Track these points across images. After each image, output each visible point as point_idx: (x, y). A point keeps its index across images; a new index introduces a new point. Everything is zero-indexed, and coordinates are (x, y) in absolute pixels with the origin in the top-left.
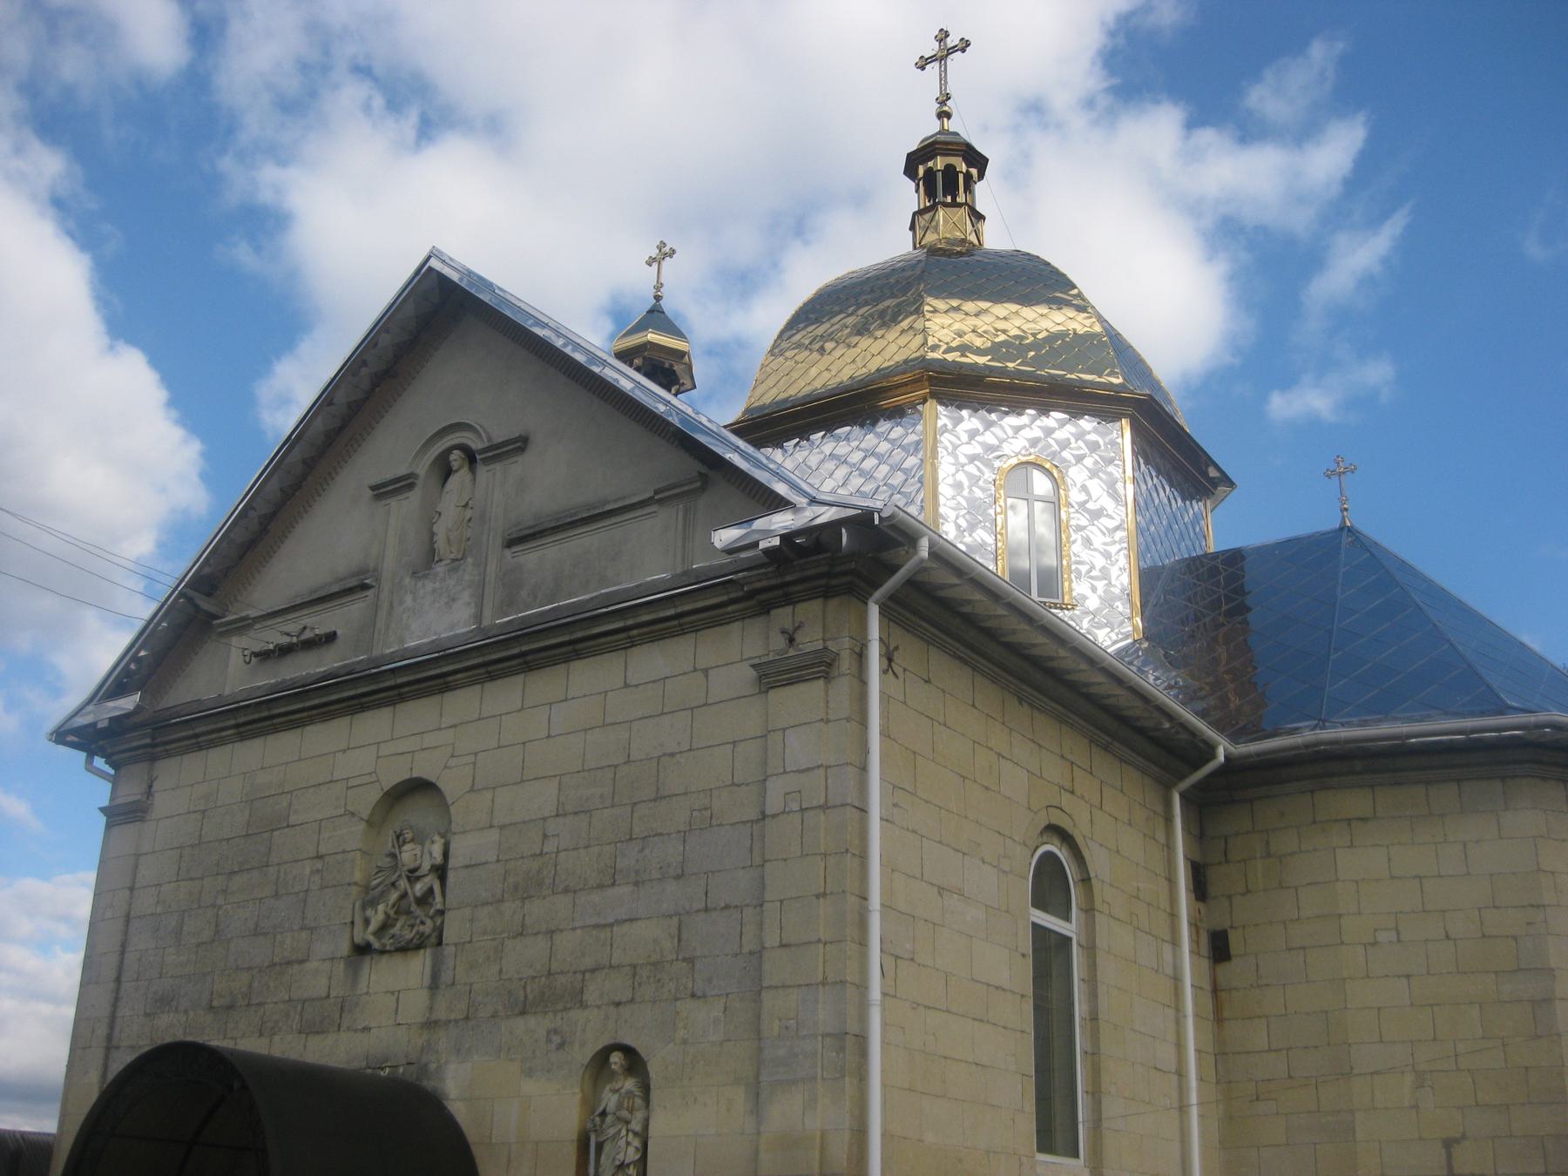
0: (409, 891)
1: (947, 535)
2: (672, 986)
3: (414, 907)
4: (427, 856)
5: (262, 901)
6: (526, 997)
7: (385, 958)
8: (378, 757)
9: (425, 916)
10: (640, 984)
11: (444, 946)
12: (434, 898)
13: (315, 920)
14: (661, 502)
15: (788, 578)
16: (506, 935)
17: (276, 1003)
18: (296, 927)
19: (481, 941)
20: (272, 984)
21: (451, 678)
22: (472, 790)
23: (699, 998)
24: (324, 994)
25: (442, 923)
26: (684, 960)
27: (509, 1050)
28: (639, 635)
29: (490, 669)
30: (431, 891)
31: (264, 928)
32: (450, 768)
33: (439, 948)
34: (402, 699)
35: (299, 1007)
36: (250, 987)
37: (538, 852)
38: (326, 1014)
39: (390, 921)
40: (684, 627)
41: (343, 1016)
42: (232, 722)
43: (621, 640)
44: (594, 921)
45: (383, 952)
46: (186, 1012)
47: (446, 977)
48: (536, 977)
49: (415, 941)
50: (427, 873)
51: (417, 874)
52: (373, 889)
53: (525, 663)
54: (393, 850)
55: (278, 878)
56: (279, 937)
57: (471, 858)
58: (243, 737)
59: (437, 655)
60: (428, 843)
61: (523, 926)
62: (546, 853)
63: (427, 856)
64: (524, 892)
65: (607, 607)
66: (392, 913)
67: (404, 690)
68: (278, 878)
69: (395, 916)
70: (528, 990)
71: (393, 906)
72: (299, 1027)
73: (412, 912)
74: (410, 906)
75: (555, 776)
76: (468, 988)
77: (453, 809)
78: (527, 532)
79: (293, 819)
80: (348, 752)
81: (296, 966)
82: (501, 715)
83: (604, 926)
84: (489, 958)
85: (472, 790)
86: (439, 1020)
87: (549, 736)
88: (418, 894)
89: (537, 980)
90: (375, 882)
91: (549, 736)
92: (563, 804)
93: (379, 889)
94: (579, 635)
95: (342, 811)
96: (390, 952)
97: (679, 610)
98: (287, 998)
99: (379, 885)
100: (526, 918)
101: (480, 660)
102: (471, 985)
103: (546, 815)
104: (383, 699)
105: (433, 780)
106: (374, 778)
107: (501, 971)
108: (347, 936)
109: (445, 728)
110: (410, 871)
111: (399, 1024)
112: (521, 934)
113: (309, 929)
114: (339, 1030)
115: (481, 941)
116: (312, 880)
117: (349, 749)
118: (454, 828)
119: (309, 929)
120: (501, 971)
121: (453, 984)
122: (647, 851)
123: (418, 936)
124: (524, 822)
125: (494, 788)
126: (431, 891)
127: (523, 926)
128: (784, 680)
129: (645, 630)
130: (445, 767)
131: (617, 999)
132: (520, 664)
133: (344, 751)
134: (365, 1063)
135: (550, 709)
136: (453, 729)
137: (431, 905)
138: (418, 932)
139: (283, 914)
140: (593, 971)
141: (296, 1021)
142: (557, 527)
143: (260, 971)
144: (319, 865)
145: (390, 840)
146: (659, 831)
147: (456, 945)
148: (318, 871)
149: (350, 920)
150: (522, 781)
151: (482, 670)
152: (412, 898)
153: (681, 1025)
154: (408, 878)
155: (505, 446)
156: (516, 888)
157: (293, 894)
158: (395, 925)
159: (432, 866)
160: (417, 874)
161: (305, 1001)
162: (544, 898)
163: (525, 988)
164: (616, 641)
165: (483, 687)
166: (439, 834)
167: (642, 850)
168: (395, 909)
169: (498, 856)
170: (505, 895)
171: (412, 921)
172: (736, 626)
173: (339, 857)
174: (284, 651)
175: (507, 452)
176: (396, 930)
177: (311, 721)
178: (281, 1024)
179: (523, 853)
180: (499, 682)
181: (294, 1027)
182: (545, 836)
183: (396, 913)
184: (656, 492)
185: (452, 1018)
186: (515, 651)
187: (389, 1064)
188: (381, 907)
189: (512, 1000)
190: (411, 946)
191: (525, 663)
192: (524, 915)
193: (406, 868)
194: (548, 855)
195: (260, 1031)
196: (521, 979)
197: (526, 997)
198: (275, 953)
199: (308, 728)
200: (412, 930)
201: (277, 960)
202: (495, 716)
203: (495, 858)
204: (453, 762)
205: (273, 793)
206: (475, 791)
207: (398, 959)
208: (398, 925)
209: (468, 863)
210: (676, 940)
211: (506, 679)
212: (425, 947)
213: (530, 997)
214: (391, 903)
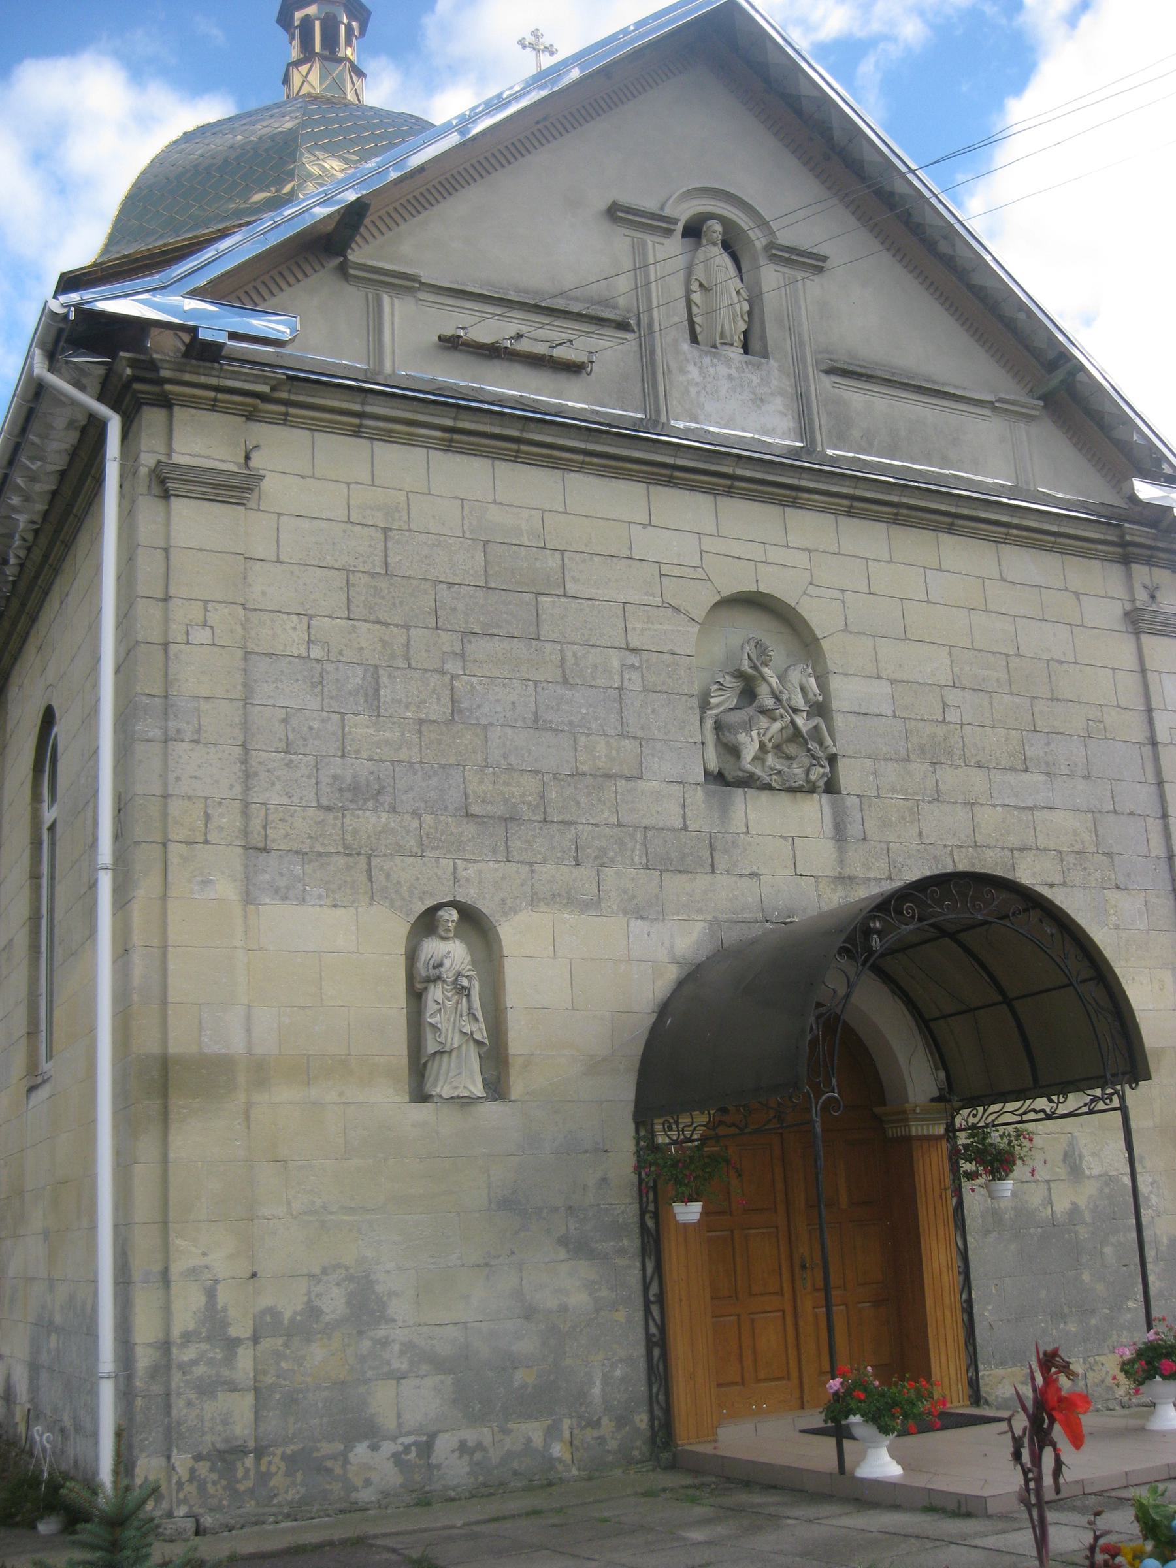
2: (1098, 875)
7: (765, 796)
10: (1068, 869)
14: (994, 409)
15: (1161, 544)
17: (597, 825)
20: (583, 800)
23: (1123, 889)
26: (1104, 854)
28: (1017, 536)
34: (729, 492)
36: (543, 797)
38: (687, 851)
42: (449, 423)
43: (999, 533)
44: (1012, 801)
45: (768, 787)
46: (416, 814)
47: (854, 829)
48: (962, 847)
58: (449, 447)
59: (891, 480)
61: (937, 791)
65: (1010, 499)
67: (524, 448)
78: (858, 370)
81: (622, 783)
83: (1024, 808)
89: (963, 850)
92: (959, 677)
94: (966, 512)
97: (1062, 530)
100: (940, 783)
101: (851, 491)
102: (888, 843)
104: (702, 482)
107: (920, 834)
111: (801, 875)
112: (937, 800)
114: (713, 872)
120: (920, 834)
122: (1053, 746)
127: (937, 791)
128: (1155, 629)
129: (1025, 534)
131: (1049, 881)
139: (584, 711)
140: (1021, 850)
142: (890, 381)
144: (633, 659)
146: (1061, 731)
151: (846, 502)
153: (1112, 912)
155: (808, 258)
163: (952, 854)
164: (878, 512)
167: (1048, 744)
172: (1096, 564)
174: (493, 352)
175: (804, 263)
177: (581, 468)
181: (636, 859)
184: (1000, 400)
186: (895, 499)
191: (896, 514)
195: (576, 859)
199: (572, 475)
201: (582, 768)
204: (812, 590)
207: (785, 798)
209: (857, 709)
210: (1094, 835)
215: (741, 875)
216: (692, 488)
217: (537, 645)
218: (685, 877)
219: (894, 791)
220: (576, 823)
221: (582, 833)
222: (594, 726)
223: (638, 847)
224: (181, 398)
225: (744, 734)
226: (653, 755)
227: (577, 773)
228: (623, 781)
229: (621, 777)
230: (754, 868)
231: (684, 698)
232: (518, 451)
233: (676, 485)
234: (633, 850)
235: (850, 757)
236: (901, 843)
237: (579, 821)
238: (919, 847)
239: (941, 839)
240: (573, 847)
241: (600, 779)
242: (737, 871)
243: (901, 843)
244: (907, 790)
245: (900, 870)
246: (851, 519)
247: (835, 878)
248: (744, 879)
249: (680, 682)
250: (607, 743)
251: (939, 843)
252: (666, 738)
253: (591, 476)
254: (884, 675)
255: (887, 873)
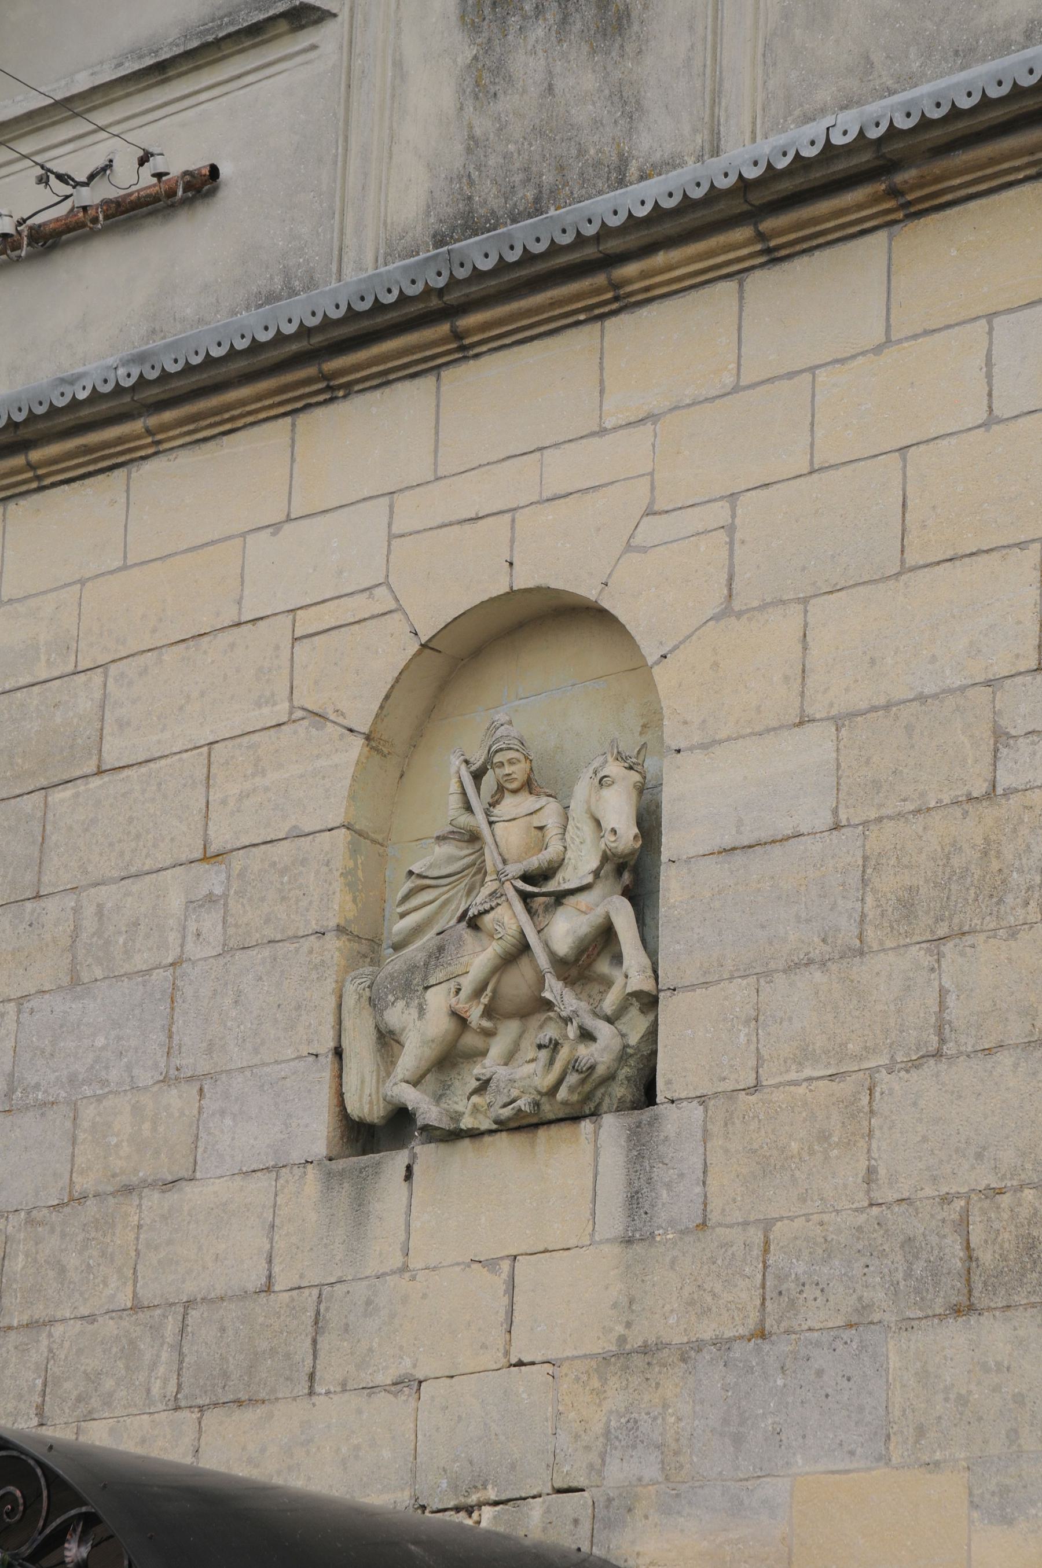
0: (532, 938)
1: (827, 462)
3: (554, 989)
4: (581, 829)
5: (27, 1006)
6: (970, 1257)
8: (391, 537)
9: (596, 1014)
11: (662, 1108)
12: (618, 959)
13: (209, 1050)
16: (884, 1060)
17: (91, 1318)
18: (145, 1078)
19: (795, 1083)
20: (72, 1261)
21: (631, 269)
22: (727, 611)
24: (255, 1279)
25: (652, 1033)
27: (921, 1431)
29: (768, 225)
30: (606, 934)
31: (37, 1087)
32: (644, 550)
33: (647, 1113)
35: (171, 1326)
37: (979, 788)
39: (470, 1040)
40: (467, 342)
41: (323, 1343)
48: (1001, 1192)
49: (562, 1094)
50: (590, 879)
51: (552, 886)
52: (397, 947)
53: (894, 192)
54: (464, 819)
55: (75, 937)
56: (89, 1113)
57: (740, 823)
60: (582, 790)
62: (1008, 793)
63: (581, 829)
64: (939, 919)
66: (475, 1014)
68: (75, 937)
69: (486, 1024)
70: (977, 1235)
71: (478, 992)
72: (172, 1388)
73: (548, 1005)
74: (541, 982)
75: (1021, 545)
76: (756, 1236)
77: (664, 678)
79: (114, 751)
80: (287, 527)
81: (153, 1199)
82: (812, 369)
84: (824, 1137)
85: (727, 611)
86: (661, 1346)
87: (991, 421)
88: (563, 946)
89: (1005, 1200)
90: (402, 926)
91: (991, 421)
93: (428, 939)
95: (281, 711)
96: (474, 1134)
98: (125, 1299)
99: (417, 931)
100: (951, 1001)
102: (767, 1225)
103: (1002, 669)
105: (588, 590)
106: (383, 601)
108: (324, 1097)
109: (615, 429)
110: (526, 878)
111: (520, 1364)
112: (938, 1054)
113: (190, 1079)
115: (795, 1083)
116: (192, 927)
117: (289, 519)
118: (672, 734)
119: (190, 1079)
121: (703, 1225)
123: (573, 1079)
124: (922, 698)
125: (805, 601)
126: (606, 934)
130: (629, 548)
132: (876, 200)
133: (275, 527)
134: (407, 1494)
135: (990, 332)
136: (649, 427)
137: (607, 983)
138: (573, 1066)
139: (100, 1041)
141: (161, 1370)
143: (30, 1222)
144: (213, 879)
145: (454, 787)
147: (702, 1099)
148: (210, 899)
149: (332, 1044)
150: (905, 569)
152: (543, 960)
154: (526, 897)
156: (907, 905)
157: (129, 975)
158: (484, 1053)
159: (605, 858)
160: (552, 886)
161: (189, 1304)
162: (1013, 933)
163: (963, 1223)
164: (992, 161)
165: (741, 285)
166: (620, 757)
168: (485, 1000)
169: (835, 812)
170: (870, 933)
171: (551, 1032)
173: (281, 852)
176: (489, 1065)
178: (109, 1384)
179: (922, 795)
180: (799, 265)
181: (156, 1390)
182: (1001, 737)
183: (489, 1012)
185: (708, 1335)
187: (492, 1495)
188: (438, 1000)
189: (918, 1268)
190: (548, 1110)
192: (943, 993)
193: (514, 869)
194: (1014, 800)
196: (946, 1199)
197: (970, 1257)
198: (79, 1160)
199: (148, 466)
200: (551, 1062)
201: (84, 1183)
202: (791, 375)
203: (826, 819)
204: (651, 530)
205: (44, 676)
206: (739, 615)
208: (497, 1048)
209: (728, 841)
211: (821, 257)
212: (595, 1114)
213: (986, 1257)
214: (468, 983)
215: (371, 1389)
216: (384, 380)
217: (34, 911)
218: (251, 1415)
219: (804, 1055)
220: (52, 1322)
221: (61, 1346)
222: (114, 1075)
223: (164, 1356)
224: (188, 439)
225: (400, 1004)
226: (223, 1113)
227: (72, 1199)
228: (156, 1195)
229: (152, 1185)
230: (405, 1366)
231: (306, 944)
232: (31, 466)
233: (348, 390)
234: (154, 1366)
235: (692, 987)
236: (807, 1217)
237: (59, 1316)
238: (862, 1218)
239: (934, 1179)
240: (39, 1382)
241: (112, 1201)
242: (366, 1379)
243: (807, 1217)
244: (843, 1045)
245: (792, 1303)
246: (786, 266)
247: (606, 1359)
248: (382, 1398)
249: (303, 904)
250: (137, 1109)
251: (929, 1191)
252: (256, 1060)
253: (183, 453)
254: (817, 710)
255: (754, 1317)
